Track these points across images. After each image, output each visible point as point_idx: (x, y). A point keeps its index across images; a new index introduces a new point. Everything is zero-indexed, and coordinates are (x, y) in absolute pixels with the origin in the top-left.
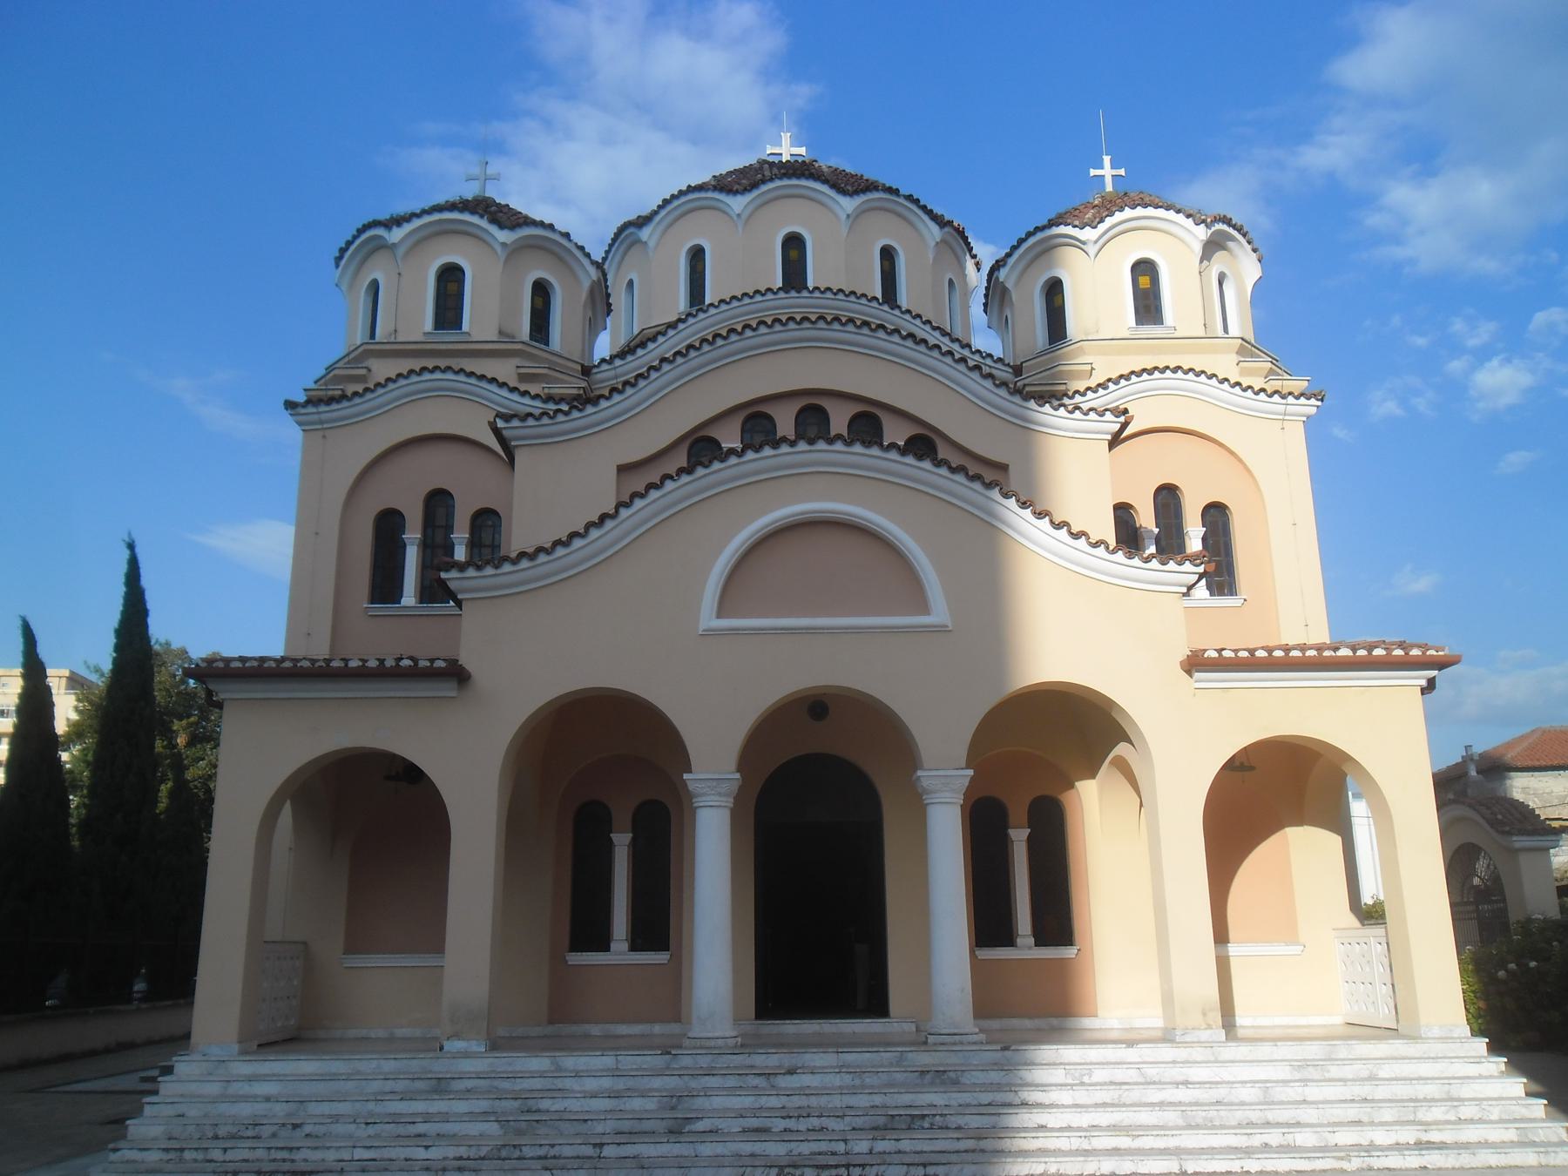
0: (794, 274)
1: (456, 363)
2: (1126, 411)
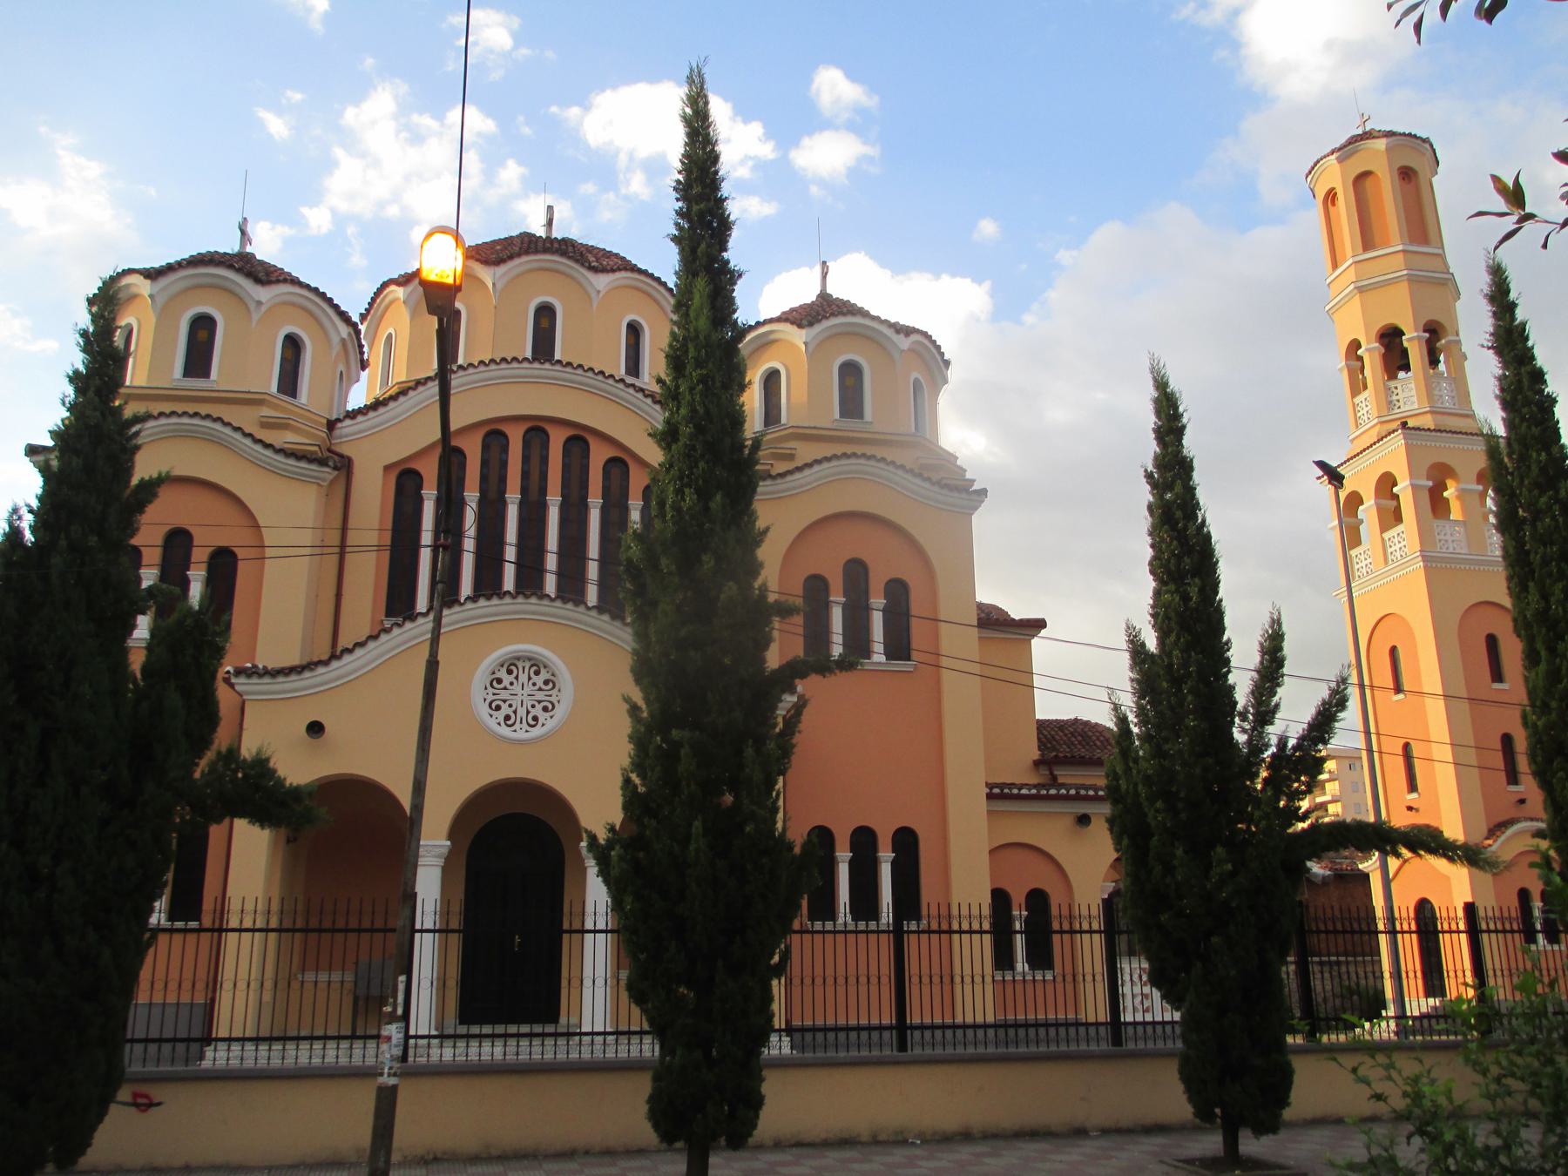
1: (204, 409)
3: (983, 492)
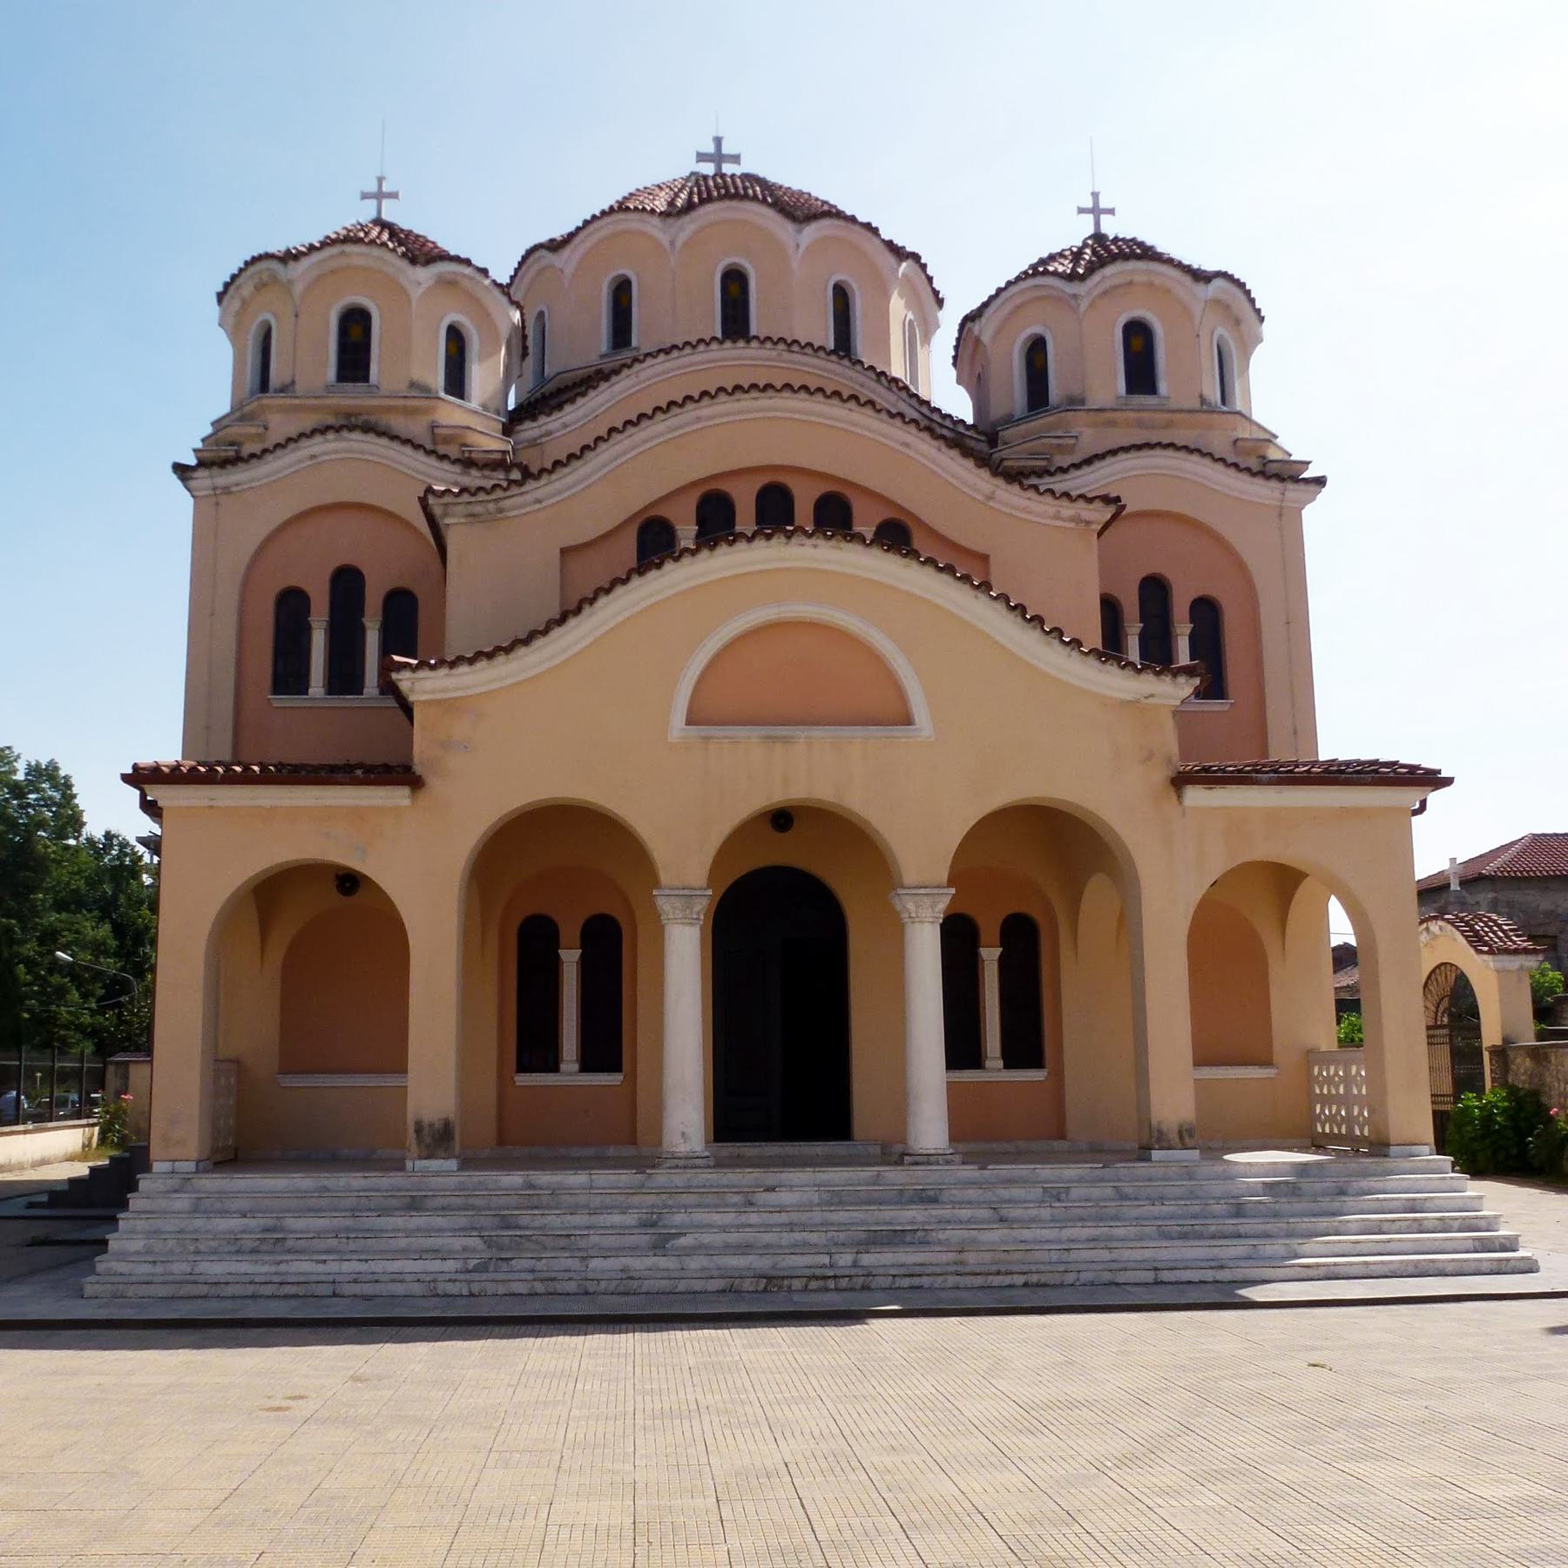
0: (735, 322)
2: (1118, 499)
3: (1320, 482)
